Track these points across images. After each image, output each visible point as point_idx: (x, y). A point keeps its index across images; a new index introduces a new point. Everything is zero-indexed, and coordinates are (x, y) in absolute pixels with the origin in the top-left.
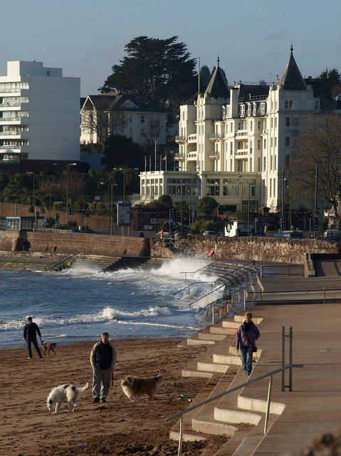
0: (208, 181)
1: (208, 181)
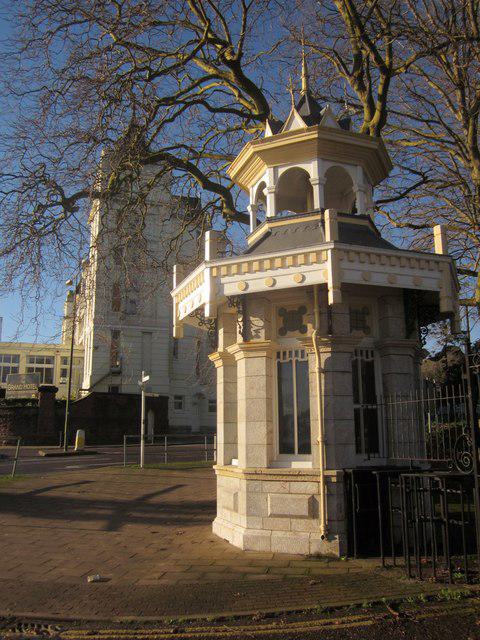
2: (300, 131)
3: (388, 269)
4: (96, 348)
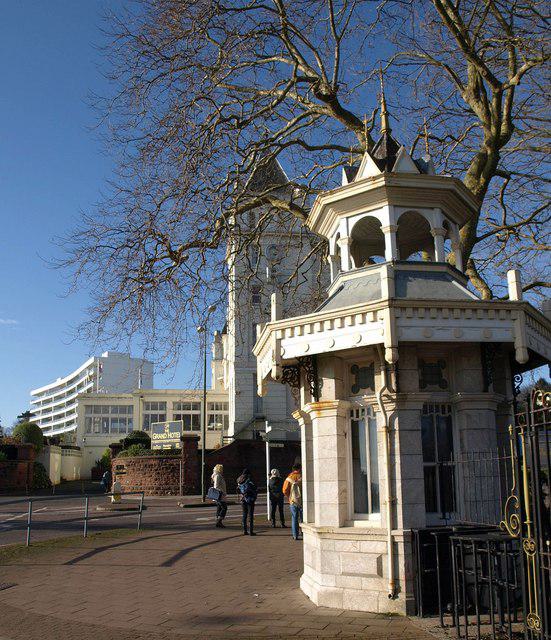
0: (147, 406)
1: (147, 406)
2: (407, 175)
3: (452, 323)
4: (238, 393)
